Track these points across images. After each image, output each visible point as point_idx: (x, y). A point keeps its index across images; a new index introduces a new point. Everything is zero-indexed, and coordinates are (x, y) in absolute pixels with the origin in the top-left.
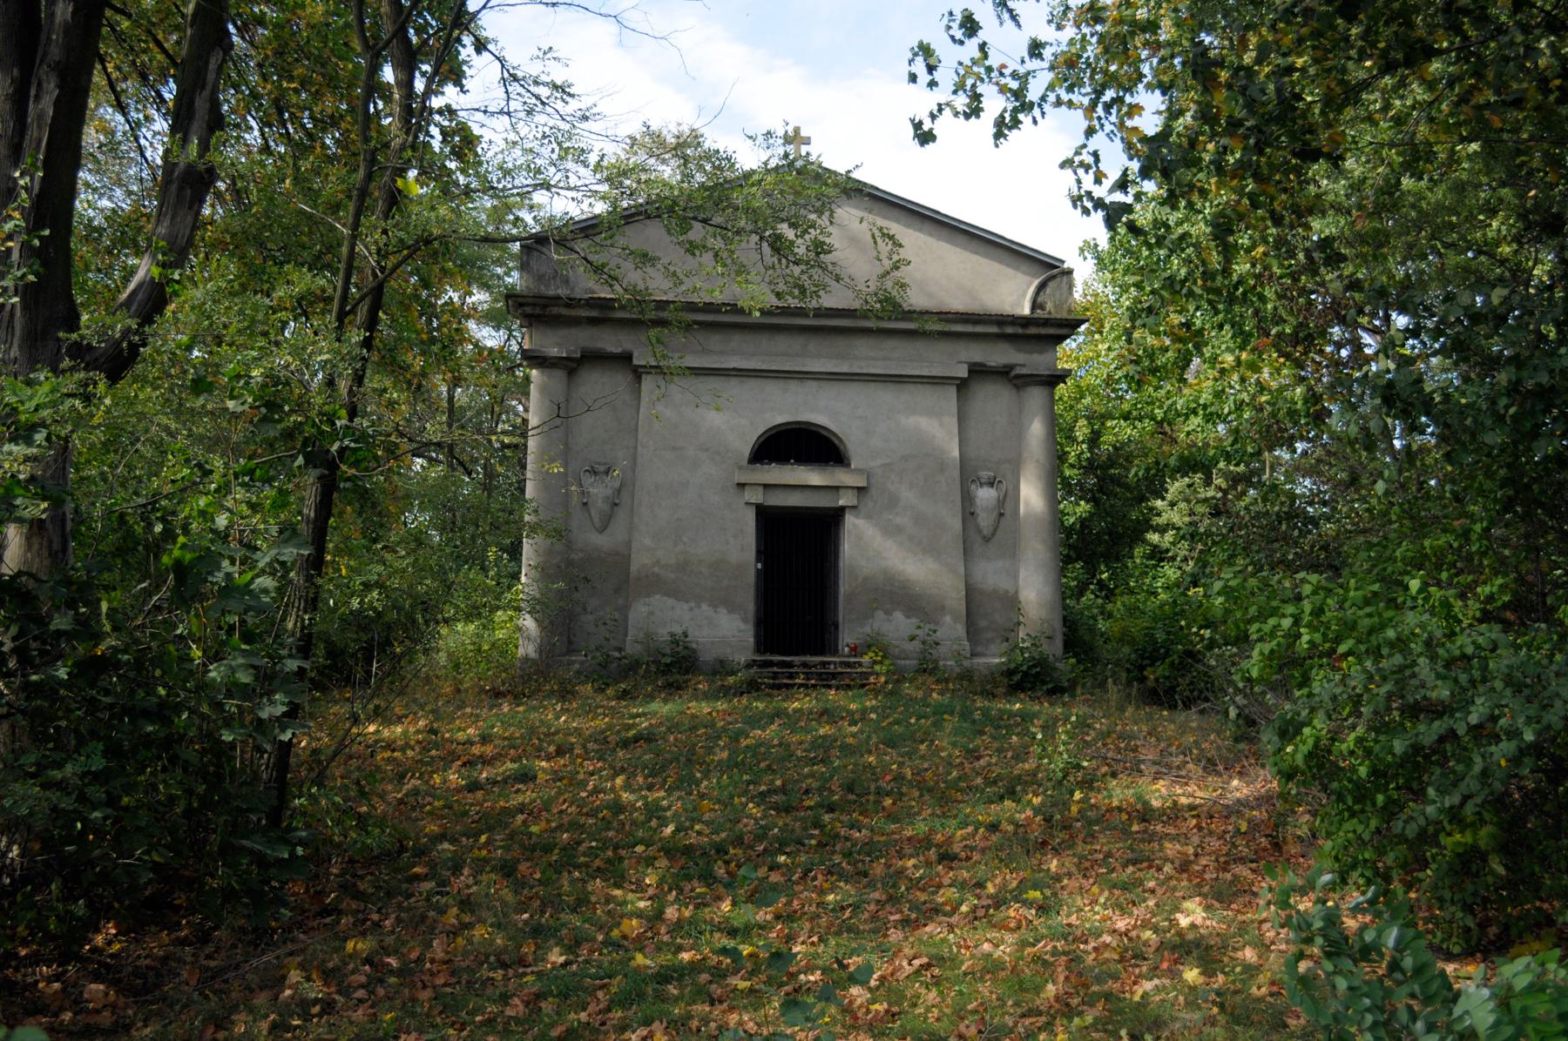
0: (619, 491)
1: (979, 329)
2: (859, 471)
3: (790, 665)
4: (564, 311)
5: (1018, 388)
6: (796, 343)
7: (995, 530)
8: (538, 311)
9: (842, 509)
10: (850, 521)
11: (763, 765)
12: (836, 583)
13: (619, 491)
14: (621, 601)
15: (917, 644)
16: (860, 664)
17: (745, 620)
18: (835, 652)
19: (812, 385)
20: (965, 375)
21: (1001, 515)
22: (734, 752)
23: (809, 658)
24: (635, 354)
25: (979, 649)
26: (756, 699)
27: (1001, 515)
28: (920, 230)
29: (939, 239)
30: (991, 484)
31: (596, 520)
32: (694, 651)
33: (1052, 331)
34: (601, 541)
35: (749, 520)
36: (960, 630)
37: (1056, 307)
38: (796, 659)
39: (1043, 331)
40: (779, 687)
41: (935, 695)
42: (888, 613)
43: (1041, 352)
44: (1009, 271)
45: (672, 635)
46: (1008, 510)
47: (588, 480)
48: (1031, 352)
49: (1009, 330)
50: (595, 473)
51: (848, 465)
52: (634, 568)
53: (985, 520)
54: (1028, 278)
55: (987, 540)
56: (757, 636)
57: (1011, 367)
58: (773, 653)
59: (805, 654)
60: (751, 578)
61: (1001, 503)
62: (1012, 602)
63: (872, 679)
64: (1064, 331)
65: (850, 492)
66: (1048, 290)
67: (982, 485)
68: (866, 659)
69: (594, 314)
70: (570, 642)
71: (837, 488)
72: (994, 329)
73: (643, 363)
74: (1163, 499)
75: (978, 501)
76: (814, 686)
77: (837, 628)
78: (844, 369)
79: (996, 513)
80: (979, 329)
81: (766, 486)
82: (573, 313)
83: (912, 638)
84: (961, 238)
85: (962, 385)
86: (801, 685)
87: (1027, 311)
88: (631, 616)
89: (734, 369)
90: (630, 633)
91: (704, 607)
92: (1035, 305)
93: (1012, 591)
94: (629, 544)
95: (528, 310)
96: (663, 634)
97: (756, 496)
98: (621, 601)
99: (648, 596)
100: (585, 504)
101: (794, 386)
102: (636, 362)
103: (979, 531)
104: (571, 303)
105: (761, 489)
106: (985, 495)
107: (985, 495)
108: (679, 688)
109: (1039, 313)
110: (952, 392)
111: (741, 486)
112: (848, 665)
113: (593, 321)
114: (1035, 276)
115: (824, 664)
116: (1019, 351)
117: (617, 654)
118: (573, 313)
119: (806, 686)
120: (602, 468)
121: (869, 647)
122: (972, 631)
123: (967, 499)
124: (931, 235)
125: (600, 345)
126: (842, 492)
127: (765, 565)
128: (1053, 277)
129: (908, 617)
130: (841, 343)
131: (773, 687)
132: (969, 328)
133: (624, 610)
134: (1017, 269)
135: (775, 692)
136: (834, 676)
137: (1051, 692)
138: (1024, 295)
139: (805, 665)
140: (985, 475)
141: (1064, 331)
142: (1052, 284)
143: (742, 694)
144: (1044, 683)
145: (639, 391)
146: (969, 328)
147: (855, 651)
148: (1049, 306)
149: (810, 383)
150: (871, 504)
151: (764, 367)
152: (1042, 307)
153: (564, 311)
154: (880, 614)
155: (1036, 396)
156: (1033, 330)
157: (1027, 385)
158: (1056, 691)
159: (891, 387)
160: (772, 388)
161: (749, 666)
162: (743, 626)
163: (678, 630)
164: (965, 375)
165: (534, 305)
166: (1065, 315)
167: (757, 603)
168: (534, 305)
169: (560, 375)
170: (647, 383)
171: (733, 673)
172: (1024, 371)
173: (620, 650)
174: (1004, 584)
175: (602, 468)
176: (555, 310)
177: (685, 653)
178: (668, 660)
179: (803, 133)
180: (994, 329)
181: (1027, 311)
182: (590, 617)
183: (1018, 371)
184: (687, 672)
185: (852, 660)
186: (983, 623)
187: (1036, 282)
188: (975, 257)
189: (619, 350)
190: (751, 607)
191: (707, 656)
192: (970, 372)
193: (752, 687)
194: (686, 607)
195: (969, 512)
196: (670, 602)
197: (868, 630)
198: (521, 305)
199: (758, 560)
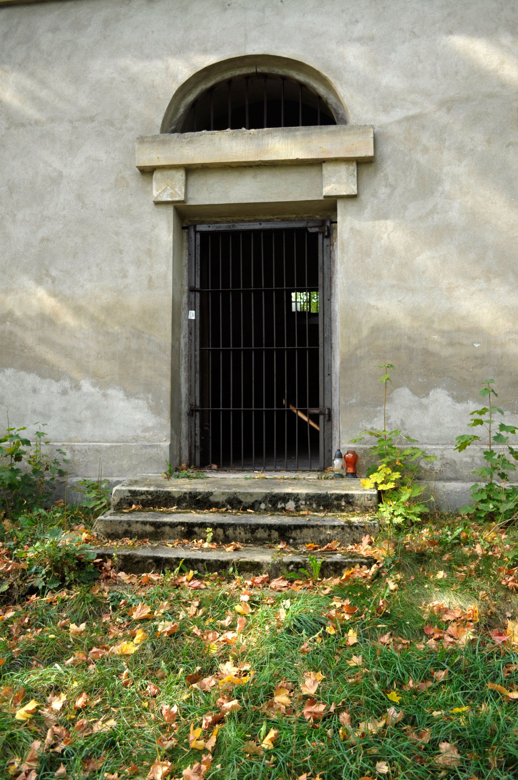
17: (155, 410)
126: (327, 169)
129: (459, 399)
150: (383, 191)
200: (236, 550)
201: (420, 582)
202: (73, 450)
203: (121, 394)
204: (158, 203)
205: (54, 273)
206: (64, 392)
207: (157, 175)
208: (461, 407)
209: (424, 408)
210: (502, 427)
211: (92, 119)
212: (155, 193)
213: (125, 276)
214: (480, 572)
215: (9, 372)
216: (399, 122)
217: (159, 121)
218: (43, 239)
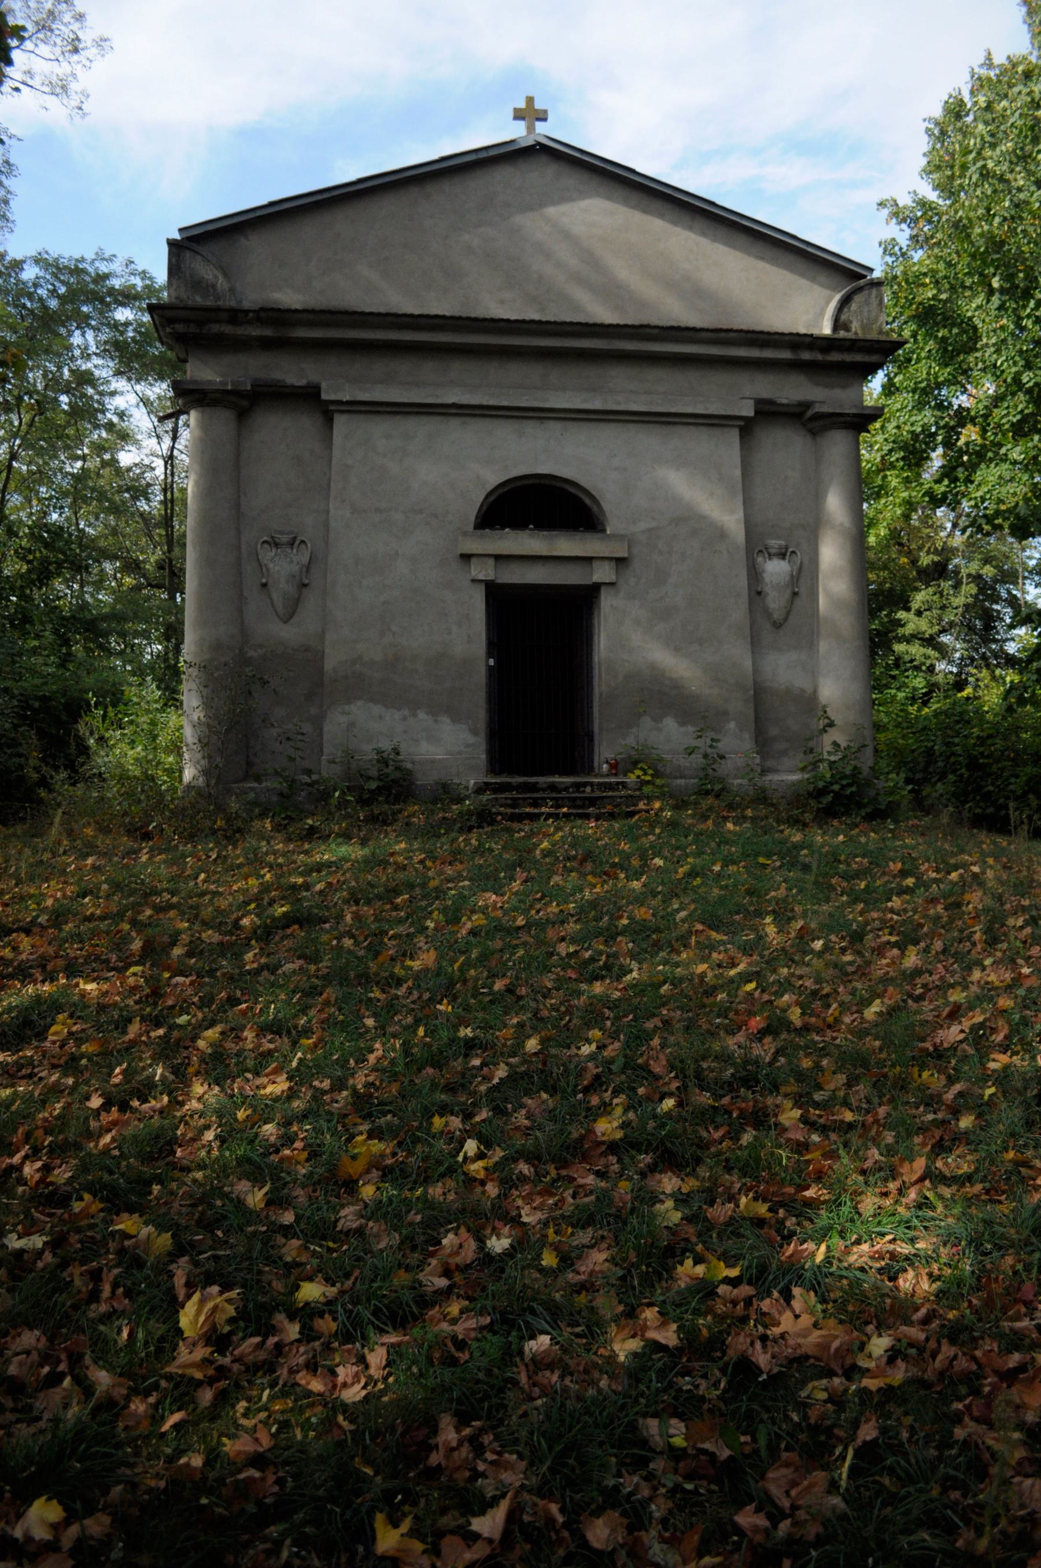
0: (308, 568)
1: (768, 354)
2: (619, 537)
3: (533, 788)
4: (227, 329)
5: (814, 433)
6: (532, 372)
7: (788, 613)
8: (193, 329)
9: (596, 588)
10: (607, 602)
11: (499, 985)
12: (590, 683)
13: (308, 568)
14: (314, 710)
15: (697, 759)
16: (624, 785)
17: (474, 732)
18: (590, 770)
19: (555, 427)
20: (751, 413)
21: (795, 594)
22: (448, 948)
23: (557, 779)
24: (324, 386)
25: (769, 763)
26: (491, 836)
27: (795, 594)
28: (690, 228)
29: (715, 240)
30: (782, 556)
31: (279, 604)
32: (410, 772)
33: (859, 358)
34: (288, 633)
35: (477, 603)
36: (747, 743)
37: (864, 327)
38: (542, 780)
39: (848, 358)
40: (520, 818)
41: (730, 826)
42: (657, 719)
43: (844, 387)
44: (804, 283)
45: (379, 752)
46: (803, 590)
47: (268, 555)
48: (832, 386)
49: (806, 356)
50: (277, 545)
51: (604, 531)
52: (329, 664)
53: (775, 601)
54: (826, 292)
55: (778, 626)
56: (491, 753)
57: (807, 405)
58: (511, 772)
59: (552, 773)
60: (479, 677)
61: (795, 579)
62: (809, 703)
63: (641, 805)
64: (874, 358)
65: (606, 563)
66: (854, 306)
67: (770, 556)
68: (631, 779)
69: (268, 332)
70: (249, 764)
71: (589, 560)
72: (786, 355)
73: (333, 397)
74: (908, 609)
75: (767, 578)
76: (565, 815)
77: (591, 740)
78: (597, 404)
79: (789, 592)
80: (768, 354)
81: (498, 558)
82: (240, 331)
83: (690, 751)
84: (742, 239)
85: (746, 428)
86: (549, 815)
87: (827, 330)
88: (326, 728)
89: (454, 405)
90: (326, 750)
91: (422, 715)
92: (838, 324)
93: (809, 690)
94: (322, 636)
95: (180, 328)
96: (367, 751)
97: (485, 571)
98: (314, 710)
99: (349, 702)
100: (264, 585)
101: (531, 428)
102: (324, 396)
103: (768, 614)
104: (236, 316)
105: (491, 562)
106: (775, 569)
107: (775, 569)
108: (385, 823)
109: (842, 334)
110: (733, 436)
111: (466, 557)
112: (610, 787)
113: (268, 345)
114: (835, 289)
115: (578, 786)
116: (817, 384)
117: (306, 779)
118: (240, 331)
119: (556, 817)
120: (285, 539)
121: (635, 764)
122: (762, 742)
123: (754, 574)
124: (703, 234)
125: (277, 375)
126: (596, 564)
127: (498, 662)
128: (860, 289)
129: (682, 724)
130: (591, 373)
131: (513, 818)
132: (754, 353)
133: (318, 722)
134: (813, 280)
135: (516, 825)
136: (592, 801)
137: (870, 817)
138: (822, 313)
139: (552, 787)
140: (775, 543)
141: (874, 358)
142: (858, 299)
143: (470, 829)
144: (860, 806)
145: (331, 428)
146: (754, 353)
147: (614, 767)
148: (855, 326)
149: (552, 424)
150: (633, 581)
151: (492, 402)
152: (847, 329)
153: (227, 329)
154: (647, 721)
155: (837, 442)
156: (835, 357)
157: (825, 429)
158: (878, 815)
159: (658, 429)
160: (503, 431)
161: (480, 790)
162: (471, 739)
163: (386, 745)
164: (751, 413)
165: (187, 321)
166: (873, 335)
167: (490, 710)
168: (187, 321)
169: (224, 418)
170: (341, 422)
171: (460, 800)
172: (825, 409)
173: (309, 772)
174: (800, 682)
175: (285, 539)
176: (216, 328)
177: (398, 774)
178: (373, 785)
179: (538, 105)
180: (786, 355)
181: (827, 330)
182: (274, 732)
183: (818, 409)
184: (397, 800)
185: (613, 780)
186: (773, 731)
187: (838, 297)
188: (761, 264)
189: (303, 382)
190: (481, 715)
191: (425, 779)
192: (756, 412)
193: (484, 818)
194: (397, 715)
195: (756, 593)
196: (377, 709)
197: (631, 741)
198: (171, 321)
199: (489, 654)
200: (931, 1001)
201: (607, 868)
202: (413, 763)
203: (448, 721)
204: (474, 581)
205: (394, 628)
206: (405, 719)
207: (474, 560)
208: (682, 729)
209: (659, 730)
210: (712, 740)
211: (421, 512)
212: (473, 573)
213: (450, 633)
214: (812, 803)
215: (360, 703)
216: (643, 532)
217: (472, 518)
218: (384, 603)
